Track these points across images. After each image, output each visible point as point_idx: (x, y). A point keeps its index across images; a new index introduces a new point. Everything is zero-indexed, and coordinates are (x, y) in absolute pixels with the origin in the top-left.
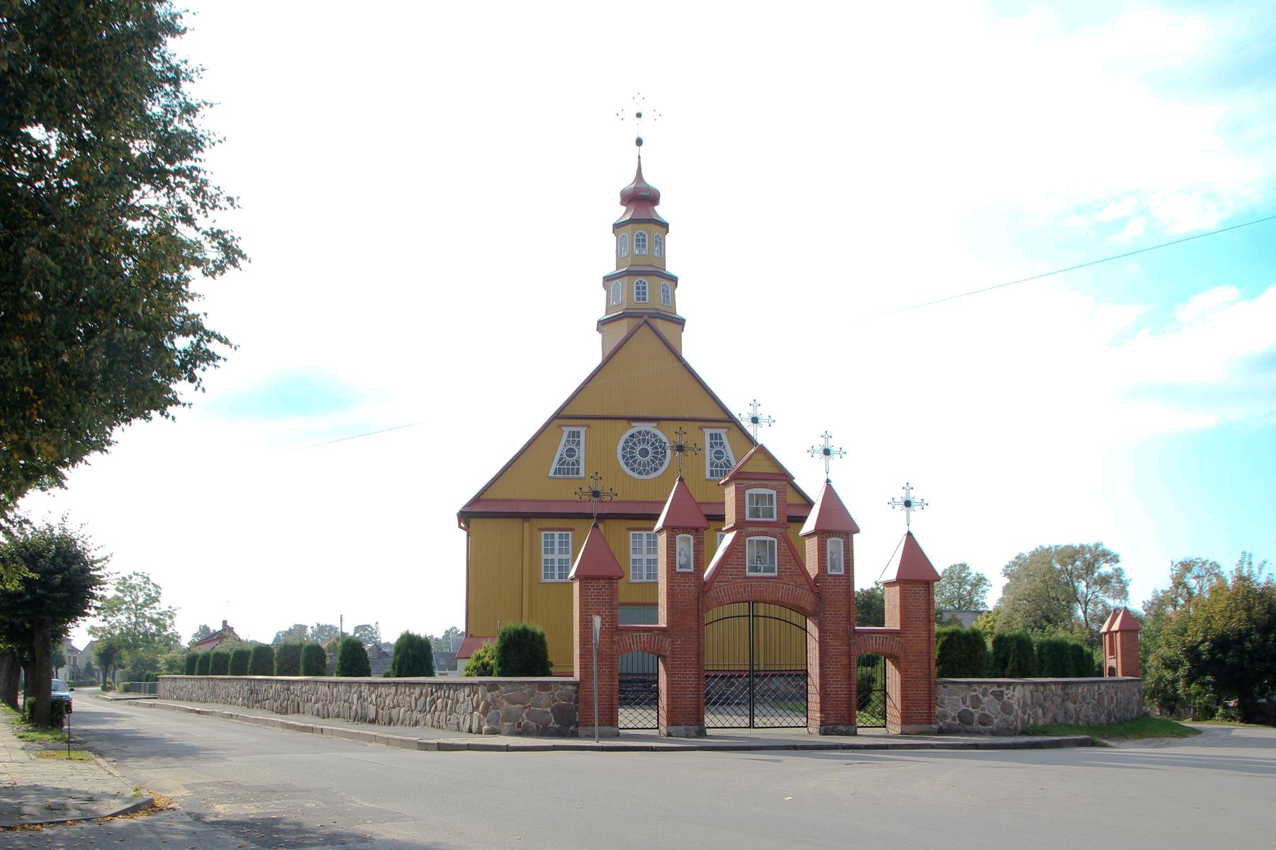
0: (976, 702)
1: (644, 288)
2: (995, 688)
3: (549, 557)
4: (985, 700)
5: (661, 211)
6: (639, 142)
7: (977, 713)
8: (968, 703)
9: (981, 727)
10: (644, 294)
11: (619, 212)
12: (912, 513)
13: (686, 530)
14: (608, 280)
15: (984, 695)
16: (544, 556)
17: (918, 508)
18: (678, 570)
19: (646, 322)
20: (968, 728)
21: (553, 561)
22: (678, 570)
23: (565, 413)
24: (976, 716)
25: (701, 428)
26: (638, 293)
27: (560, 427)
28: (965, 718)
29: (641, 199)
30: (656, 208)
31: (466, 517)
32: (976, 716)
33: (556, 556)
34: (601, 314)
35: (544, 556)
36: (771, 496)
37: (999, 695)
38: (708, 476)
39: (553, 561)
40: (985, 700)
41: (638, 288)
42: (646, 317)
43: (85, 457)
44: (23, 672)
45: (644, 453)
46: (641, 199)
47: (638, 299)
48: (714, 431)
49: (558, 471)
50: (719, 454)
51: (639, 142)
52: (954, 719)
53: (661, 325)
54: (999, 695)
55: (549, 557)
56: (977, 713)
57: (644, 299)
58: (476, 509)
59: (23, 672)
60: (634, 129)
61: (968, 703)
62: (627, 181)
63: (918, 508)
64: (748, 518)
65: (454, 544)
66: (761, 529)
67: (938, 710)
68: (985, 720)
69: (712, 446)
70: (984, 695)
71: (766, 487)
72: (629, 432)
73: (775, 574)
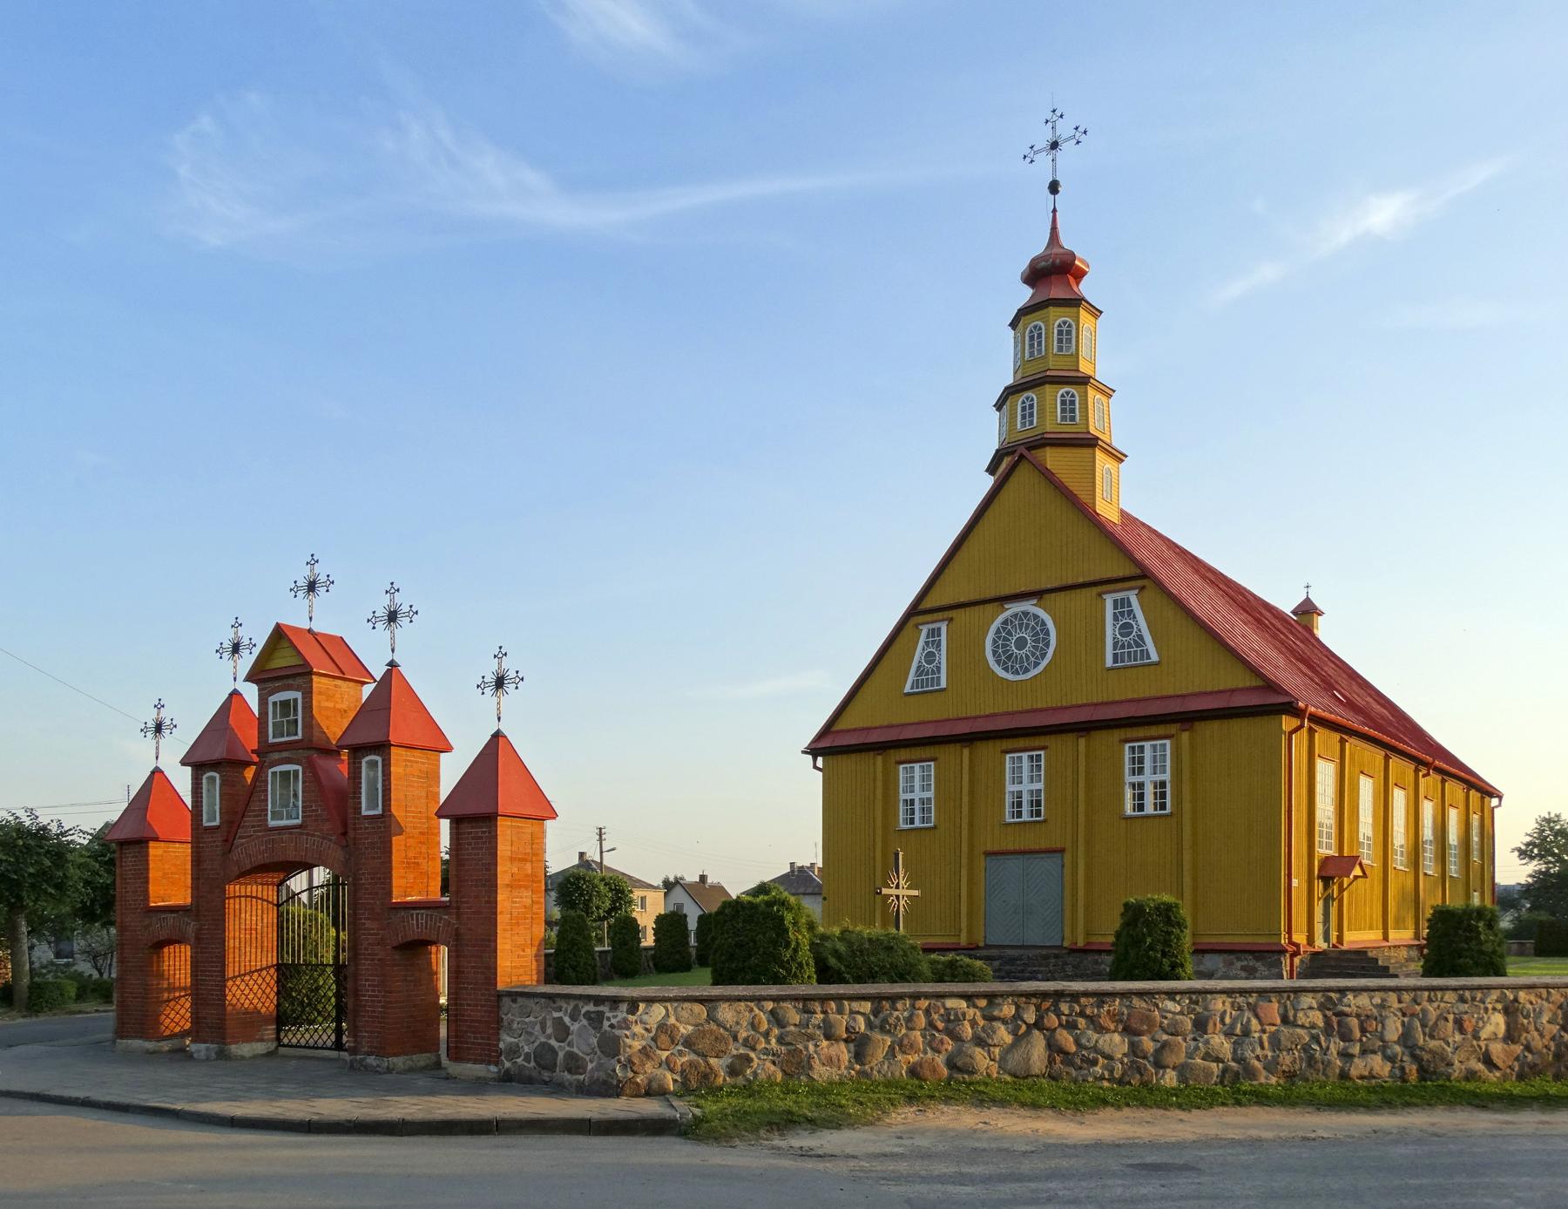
0: (563, 1032)
1: (1072, 403)
2: (591, 1007)
3: (909, 796)
5: (1086, 288)
6: (1054, 188)
7: (561, 1049)
8: (549, 1031)
9: (567, 1076)
10: (1073, 411)
13: (214, 765)
19: (1022, 457)
20: (546, 1075)
21: (912, 801)
23: (928, 604)
25: (1100, 595)
26: (1063, 411)
27: (917, 626)
28: (545, 1057)
29: (1054, 275)
31: (814, 751)
32: (561, 1054)
33: (1026, 787)
37: (596, 1020)
38: (1109, 662)
39: (912, 801)
40: (575, 1027)
41: (1063, 403)
42: (1022, 450)
45: (1021, 643)
46: (1054, 275)
47: (1064, 418)
48: (1119, 596)
49: (916, 684)
50: (1126, 629)
51: (1054, 188)
52: (527, 1058)
53: (1053, 459)
54: (596, 1020)
57: (1073, 419)
58: (821, 745)
60: (1043, 169)
61: (549, 1031)
64: (271, 740)
65: (809, 782)
66: (285, 754)
67: (506, 1040)
68: (574, 1064)
69: (1116, 618)
70: (574, 1018)
71: (289, 688)
72: (1001, 619)
73: (298, 821)
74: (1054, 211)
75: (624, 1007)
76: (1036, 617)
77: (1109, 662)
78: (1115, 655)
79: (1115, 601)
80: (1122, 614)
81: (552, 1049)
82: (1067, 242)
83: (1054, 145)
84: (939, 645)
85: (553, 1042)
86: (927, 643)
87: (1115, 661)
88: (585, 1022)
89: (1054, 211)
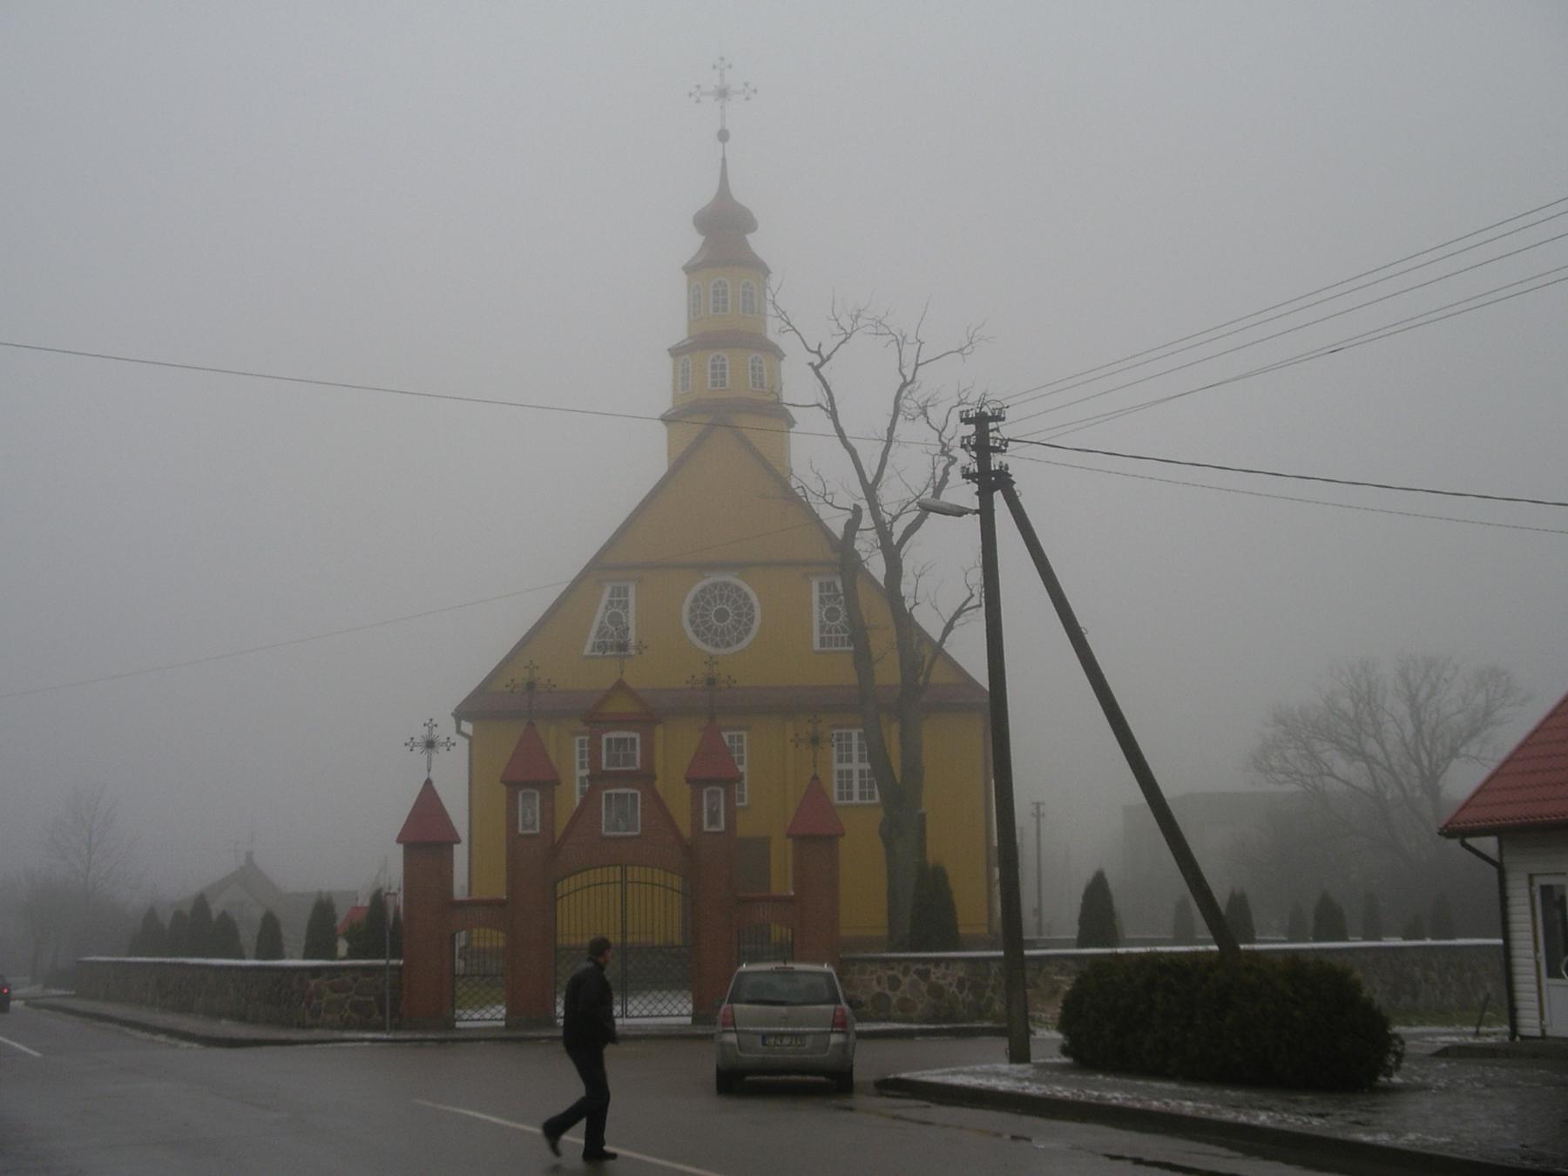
0: (895, 983)
1: (723, 367)
2: (920, 966)
3: (845, 766)
4: (906, 981)
6: (723, 136)
7: (895, 997)
11: (691, 243)
12: (435, 756)
14: (675, 352)
15: (905, 973)
16: (837, 766)
17: (442, 750)
18: (521, 831)
21: (850, 773)
22: (521, 831)
24: (894, 1001)
30: (748, 237)
32: (894, 1001)
34: (665, 404)
35: (837, 766)
36: (633, 740)
37: (925, 975)
38: (817, 646)
39: (850, 773)
41: (714, 367)
43: (907, 606)
44: (36, 1054)
51: (723, 136)
55: (845, 766)
56: (895, 997)
59: (36, 1054)
62: (704, 195)
63: (442, 750)
70: (905, 973)
74: (724, 160)
75: (943, 965)
76: (738, 589)
77: (587, 650)
78: (822, 639)
79: (821, 584)
80: (829, 598)
81: (886, 996)
82: (740, 194)
83: (723, 93)
84: (626, 606)
85: (888, 992)
86: (611, 603)
87: (822, 645)
88: (915, 977)
89: (724, 160)
